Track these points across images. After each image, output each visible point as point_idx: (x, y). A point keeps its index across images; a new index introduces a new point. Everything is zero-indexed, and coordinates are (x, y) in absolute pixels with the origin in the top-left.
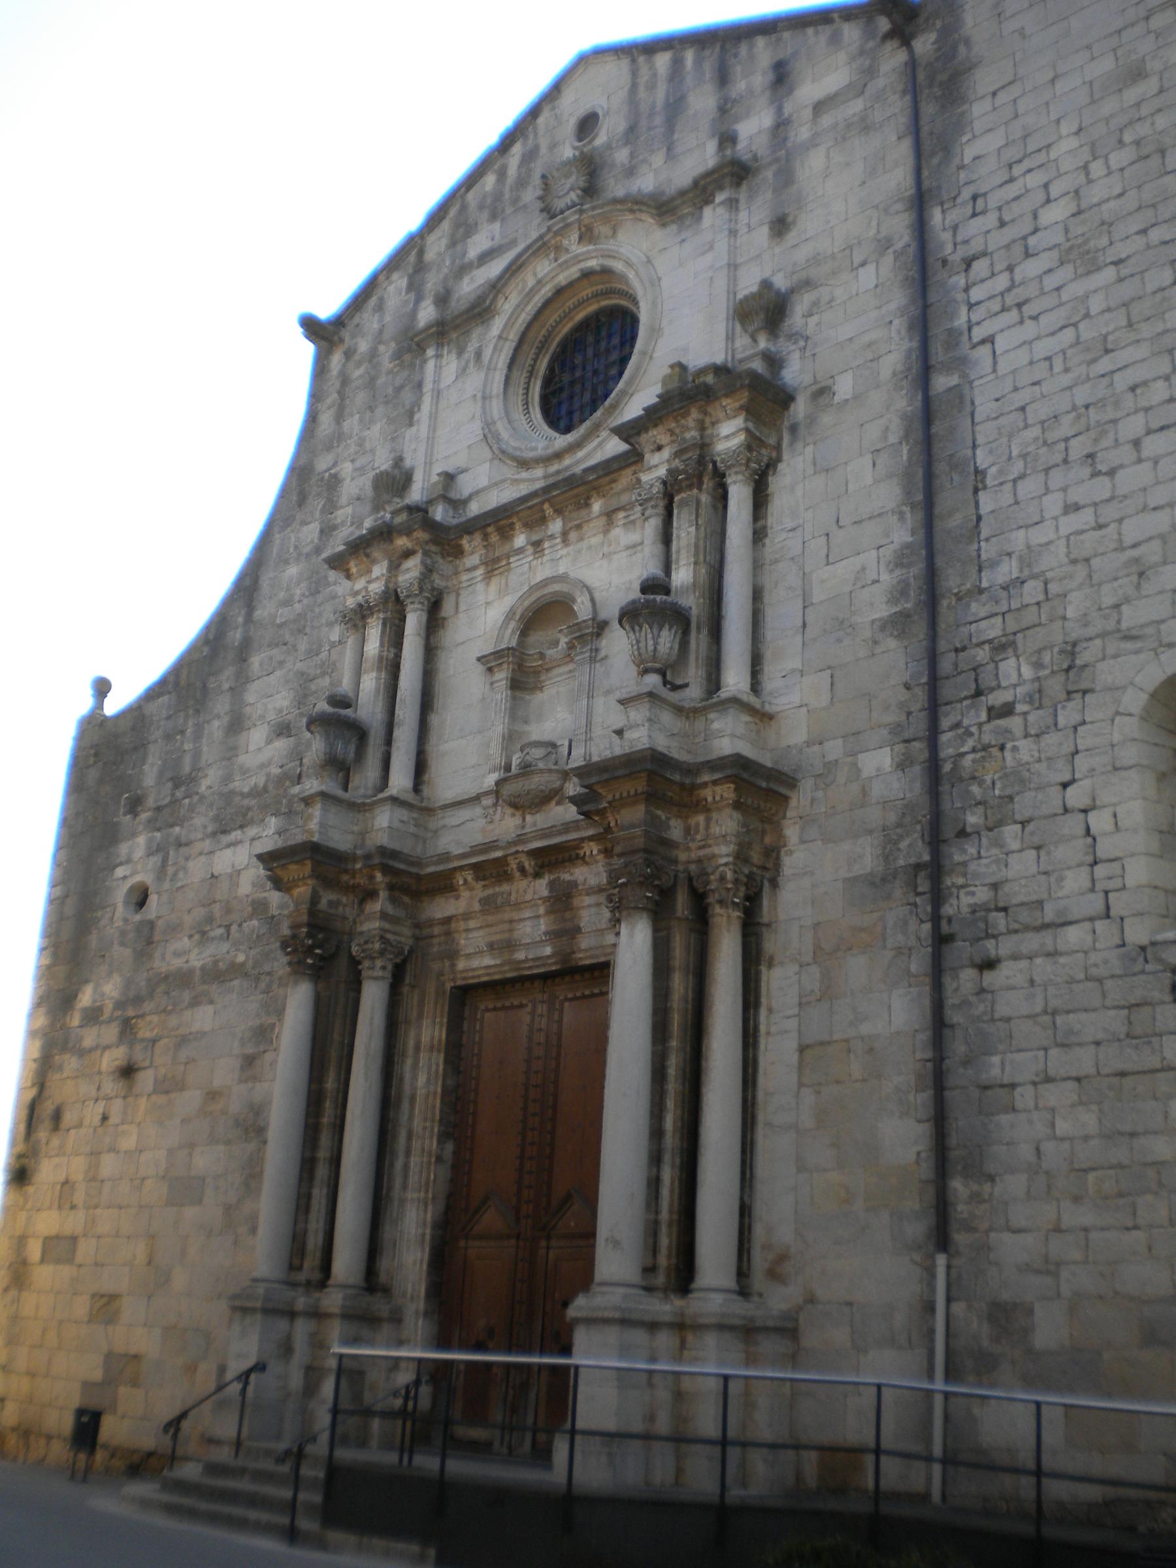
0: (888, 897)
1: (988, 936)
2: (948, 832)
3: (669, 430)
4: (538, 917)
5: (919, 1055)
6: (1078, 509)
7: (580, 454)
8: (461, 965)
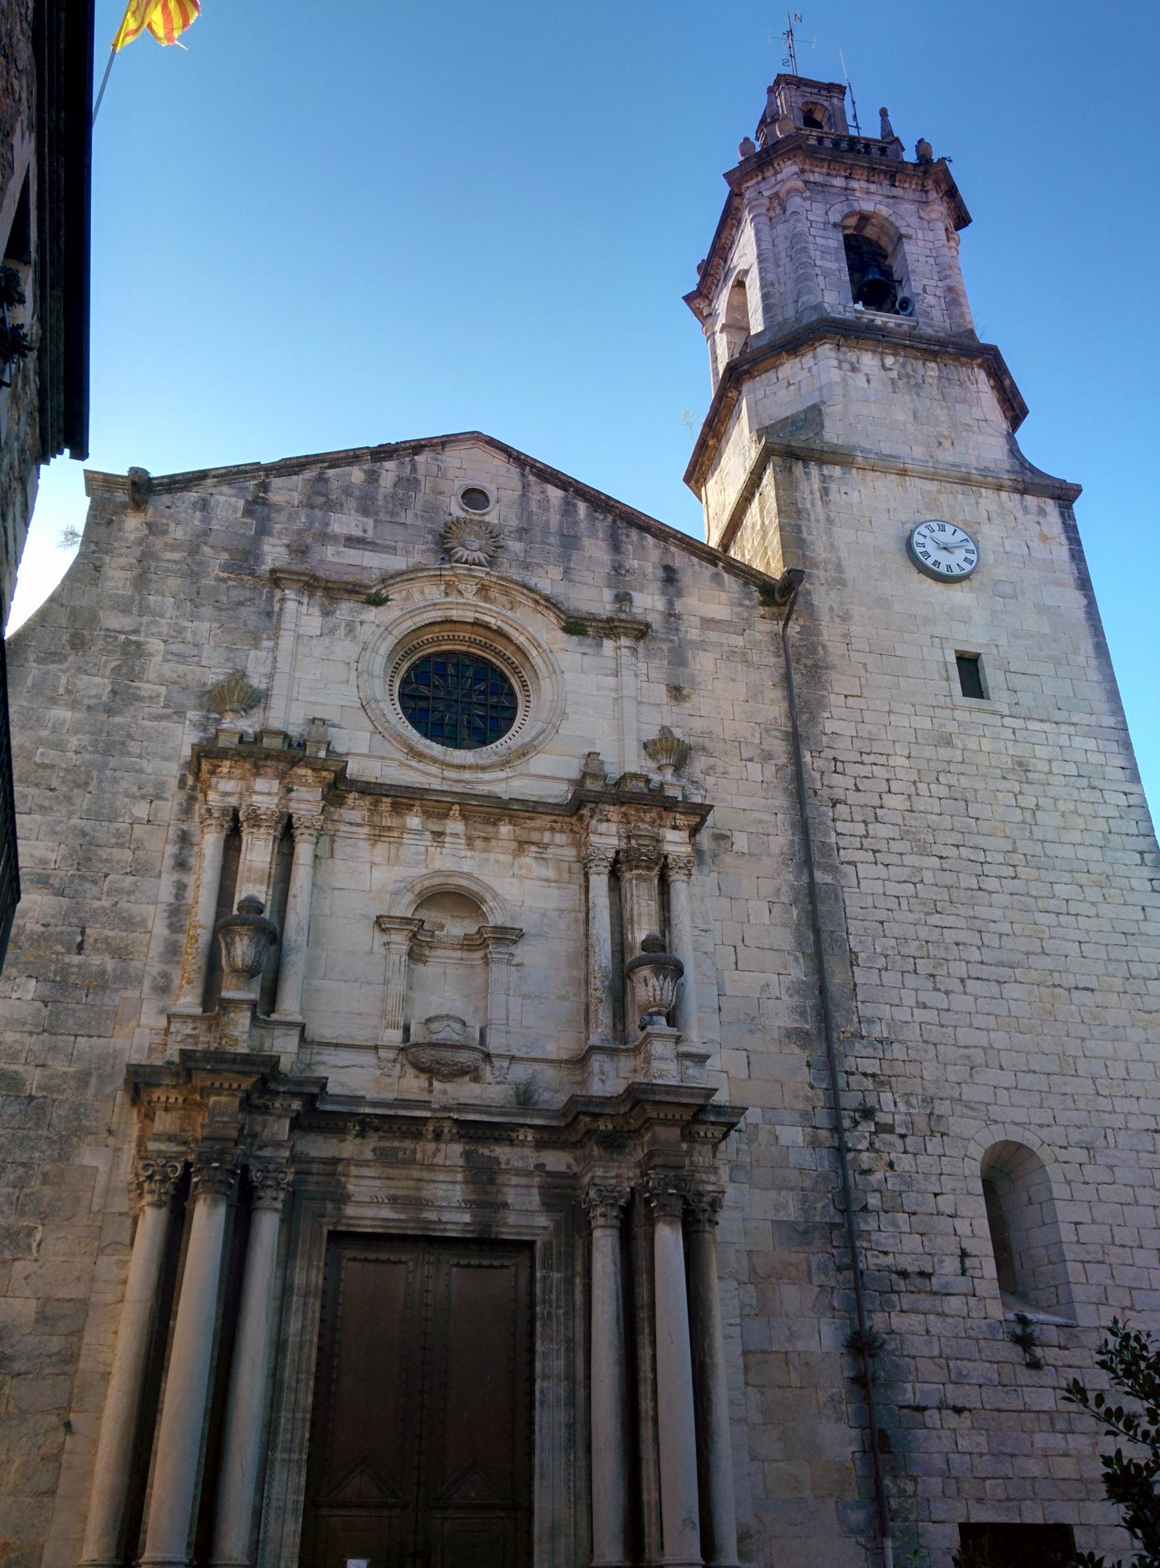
0: (811, 1243)
1: (893, 1291)
2: (855, 1207)
3: (625, 814)
4: (455, 1182)
5: (846, 1374)
6: (925, 1008)
7: (486, 776)
8: (350, 1211)
